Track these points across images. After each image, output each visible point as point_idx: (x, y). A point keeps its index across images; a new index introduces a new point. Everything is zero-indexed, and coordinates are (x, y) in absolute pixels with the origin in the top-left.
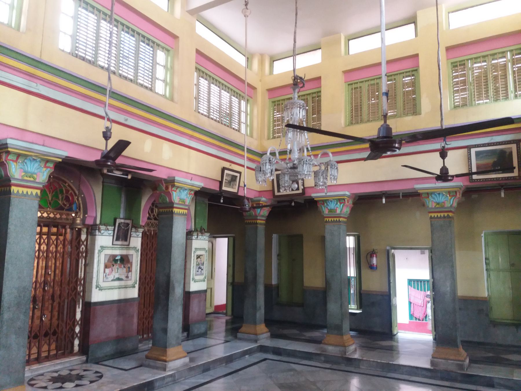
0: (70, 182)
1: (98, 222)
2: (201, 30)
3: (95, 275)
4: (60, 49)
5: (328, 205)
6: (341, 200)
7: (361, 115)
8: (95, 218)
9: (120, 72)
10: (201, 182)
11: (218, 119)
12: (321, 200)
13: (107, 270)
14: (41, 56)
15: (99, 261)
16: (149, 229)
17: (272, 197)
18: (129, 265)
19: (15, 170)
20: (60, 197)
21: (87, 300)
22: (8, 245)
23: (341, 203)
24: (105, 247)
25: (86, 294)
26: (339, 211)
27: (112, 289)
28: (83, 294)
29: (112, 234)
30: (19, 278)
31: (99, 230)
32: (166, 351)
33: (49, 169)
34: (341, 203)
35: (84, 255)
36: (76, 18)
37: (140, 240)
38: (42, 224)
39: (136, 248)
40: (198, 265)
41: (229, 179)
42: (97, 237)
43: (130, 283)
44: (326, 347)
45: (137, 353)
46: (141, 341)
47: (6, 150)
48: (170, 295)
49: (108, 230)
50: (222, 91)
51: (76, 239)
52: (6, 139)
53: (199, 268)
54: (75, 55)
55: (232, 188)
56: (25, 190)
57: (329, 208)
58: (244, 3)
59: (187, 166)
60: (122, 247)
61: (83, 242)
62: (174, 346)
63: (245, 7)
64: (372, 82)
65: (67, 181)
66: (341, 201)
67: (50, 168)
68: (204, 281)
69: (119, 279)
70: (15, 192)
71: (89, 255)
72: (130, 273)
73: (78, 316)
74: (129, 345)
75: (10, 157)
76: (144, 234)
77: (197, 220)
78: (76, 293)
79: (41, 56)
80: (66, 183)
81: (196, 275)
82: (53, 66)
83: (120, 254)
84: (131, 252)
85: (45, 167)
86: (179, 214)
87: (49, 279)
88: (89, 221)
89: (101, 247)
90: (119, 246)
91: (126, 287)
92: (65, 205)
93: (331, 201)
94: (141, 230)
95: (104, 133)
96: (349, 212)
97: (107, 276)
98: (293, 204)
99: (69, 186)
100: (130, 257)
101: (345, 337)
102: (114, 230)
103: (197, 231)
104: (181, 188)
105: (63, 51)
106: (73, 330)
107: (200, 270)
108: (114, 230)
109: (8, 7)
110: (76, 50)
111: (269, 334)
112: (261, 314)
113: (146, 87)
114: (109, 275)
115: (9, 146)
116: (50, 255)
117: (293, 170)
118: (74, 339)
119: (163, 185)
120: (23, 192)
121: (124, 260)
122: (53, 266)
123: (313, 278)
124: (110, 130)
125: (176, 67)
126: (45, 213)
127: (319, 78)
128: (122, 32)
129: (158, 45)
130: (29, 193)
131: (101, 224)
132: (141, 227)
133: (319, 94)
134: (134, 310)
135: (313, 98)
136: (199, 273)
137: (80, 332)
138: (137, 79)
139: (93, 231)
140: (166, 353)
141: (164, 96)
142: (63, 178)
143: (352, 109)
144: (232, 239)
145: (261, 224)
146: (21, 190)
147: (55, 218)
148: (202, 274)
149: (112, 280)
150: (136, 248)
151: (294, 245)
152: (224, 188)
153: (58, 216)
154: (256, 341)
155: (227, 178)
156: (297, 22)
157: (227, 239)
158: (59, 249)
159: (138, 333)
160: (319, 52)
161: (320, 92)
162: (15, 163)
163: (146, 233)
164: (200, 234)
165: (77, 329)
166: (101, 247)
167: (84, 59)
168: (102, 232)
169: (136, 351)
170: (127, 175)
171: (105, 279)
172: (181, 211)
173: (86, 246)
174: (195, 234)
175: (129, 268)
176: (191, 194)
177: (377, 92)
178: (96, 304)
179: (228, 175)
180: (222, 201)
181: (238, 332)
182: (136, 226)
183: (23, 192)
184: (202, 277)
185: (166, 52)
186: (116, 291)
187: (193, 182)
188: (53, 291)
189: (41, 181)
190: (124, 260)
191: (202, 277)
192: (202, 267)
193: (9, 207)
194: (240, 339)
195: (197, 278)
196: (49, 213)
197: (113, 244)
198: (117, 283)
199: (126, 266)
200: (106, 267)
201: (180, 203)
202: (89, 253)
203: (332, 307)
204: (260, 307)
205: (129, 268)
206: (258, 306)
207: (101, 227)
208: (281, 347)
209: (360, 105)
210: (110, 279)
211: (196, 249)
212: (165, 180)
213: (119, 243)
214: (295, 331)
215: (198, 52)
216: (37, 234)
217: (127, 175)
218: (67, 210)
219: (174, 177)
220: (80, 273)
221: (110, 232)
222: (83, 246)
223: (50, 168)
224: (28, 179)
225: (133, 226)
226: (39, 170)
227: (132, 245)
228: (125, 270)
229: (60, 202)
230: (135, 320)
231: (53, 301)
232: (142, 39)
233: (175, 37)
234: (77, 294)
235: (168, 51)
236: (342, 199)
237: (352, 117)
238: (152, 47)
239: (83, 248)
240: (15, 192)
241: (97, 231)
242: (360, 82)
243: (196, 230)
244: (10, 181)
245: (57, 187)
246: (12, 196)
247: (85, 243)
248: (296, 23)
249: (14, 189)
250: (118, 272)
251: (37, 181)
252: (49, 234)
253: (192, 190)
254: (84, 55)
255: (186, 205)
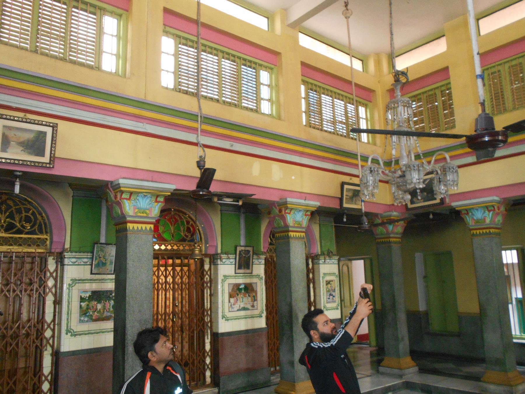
0: (191, 214)
1: (219, 251)
2: (305, 41)
3: (220, 306)
4: (163, 87)
5: (473, 215)
6: (488, 208)
7: (504, 104)
8: (216, 247)
9: (224, 99)
10: (318, 201)
11: (333, 131)
12: (463, 209)
13: (232, 300)
14: (145, 97)
15: (223, 291)
16: (271, 254)
17: (405, 211)
18: (254, 294)
19: (129, 208)
20: (182, 229)
21: (214, 331)
22: (128, 280)
23: (489, 211)
24: (228, 276)
25: (214, 325)
26: (488, 221)
27: (239, 319)
28: (211, 325)
29: (234, 263)
30: (140, 311)
31: (221, 259)
32: (294, 385)
33: (160, 204)
34: (489, 211)
35: (209, 285)
36: (177, 55)
37: (262, 267)
38: (166, 257)
39: (259, 276)
40: (328, 291)
41: (350, 194)
42: (219, 266)
43: (256, 312)
44: (485, 385)
45: (270, 386)
46: (273, 374)
47: (119, 190)
48: (294, 325)
49: (229, 258)
50: (335, 100)
51: (200, 269)
52: (118, 179)
53: (331, 295)
54: (179, 90)
55: (356, 204)
56: (140, 226)
57: (475, 218)
58: (344, 4)
59: (298, 184)
60: (245, 275)
61: (207, 273)
62: (303, 381)
63: (345, 8)
64: (514, 63)
65: (188, 213)
66: (490, 209)
67: (161, 202)
68: (337, 309)
69: (244, 309)
70: (131, 228)
71: (213, 285)
72: (256, 302)
73: (208, 347)
74: (261, 378)
75: (124, 196)
76: (266, 259)
77: (323, 242)
78: (203, 324)
79: (145, 97)
80: (186, 214)
81: (327, 303)
82: (160, 105)
83: (244, 282)
84: (254, 280)
85: (156, 201)
86: (296, 238)
87: (177, 310)
88: (211, 251)
89: (224, 276)
90: (242, 275)
91: (252, 317)
92: (187, 236)
93: (477, 210)
94: (263, 257)
95: (198, 163)
96: (501, 221)
97: (233, 306)
98: (431, 216)
99: (190, 217)
100: (254, 286)
101: (511, 374)
102: (235, 259)
103: (324, 254)
104: (296, 209)
105: (167, 88)
106: (204, 361)
107: (331, 297)
108: (235, 259)
109: (114, 57)
110: (180, 85)
111: (416, 369)
112: (404, 345)
113: (252, 110)
114: (234, 304)
115: (121, 185)
116: (176, 286)
117: (402, 179)
118: (205, 370)
119: (276, 208)
120: (138, 228)
121: (249, 289)
122: (180, 297)
123: (467, 303)
124: (204, 158)
125: (281, 83)
126: (163, 246)
127: (446, 69)
128: (223, 60)
129: (261, 65)
130: (144, 229)
131: (222, 253)
132: (263, 253)
133: (449, 86)
134: (263, 341)
135: (442, 92)
136: (331, 300)
137: (211, 363)
138: (241, 103)
139: (215, 261)
140: (295, 389)
141: (271, 116)
142: (183, 210)
143: (492, 98)
144: (368, 262)
145: (395, 243)
146: (136, 226)
147: (178, 250)
148: (335, 302)
149: (238, 310)
150: (259, 276)
151: (442, 262)
152: (345, 205)
153: (181, 248)
154: (401, 376)
155: (347, 194)
156: (393, 12)
157: (362, 261)
158: (184, 280)
159: (269, 365)
160: (443, 40)
161: (449, 83)
162: (129, 201)
163: (268, 261)
164: (327, 258)
165: (208, 361)
166: (224, 276)
167: (186, 93)
168: (224, 260)
169: (269, 384)
170: (238, 202)
171: (230, 309)
172: (298, 234)
173: (210, 276)
174: (322, 258)
175: (254, 296)
176: (308, 215)
177: (522, 73)
178: (223, 334)
179: (348, 190)
180: (345, 220)
181: (380, 366)
182: (257, 253)
183: (138, 228)
184: (334, 305)
185: (270, 70)
186: (243, 321)
187: (307, 202)
188: (182, 322)
189: (153, 216)
190: (249, 289)
191: (334, 305)
192: (333, 293)
193: (127, 243)
194: (382, 374)
195: (329, 305)
196: (172, 245)
197: (235, 273)
198: (242, 313)
199: (251, 294)
200: (231, 296)
201: (296, 225)
202: (213, 282)
203: (491, 338)
204: (403, 339)
205: (254, 296)
206: (400, 336)
207: (222, 256)
208: (431, 384)
209: (502, 92)
210: (236, 309)
211: (325, 274)
212: (277, 202)
213: (242, 271)
214: (451, 365)
215: (303, 64)
216: (154, 267)
217: (238, 202)
218: (189, 241)
219: (286, 199)
220: (206, 304)
221: (231, 260)
222: (207, 276)
223: (161, 202)
224: (142, 215)
225: (254, 253)
226: (150, 206)
227: (255, 273)
228: (250, 299)
229: (182, 234)
230: (265, 352)
231: (182, 331)
232: (244, 62)
233: (276, 54)
234: (204, 324)
235: (272, 69)
236: (490, 206)
237: (493, 107)
238: (254, 69)
239: (207, 278)
240: (131, 228)
241: (219, 260)
242: (498, 65)
243: (323, 254)
244: (126, 218)
245: (179, 219)
246: (128, 232)
247: (209, 273)
248: (391, 14)
249: (130, 226)
250: (243, 301)
251: (150, 216)
252: (174, 265)
253: (307, 211)
254: (187, 89)
255: (303, 228)
